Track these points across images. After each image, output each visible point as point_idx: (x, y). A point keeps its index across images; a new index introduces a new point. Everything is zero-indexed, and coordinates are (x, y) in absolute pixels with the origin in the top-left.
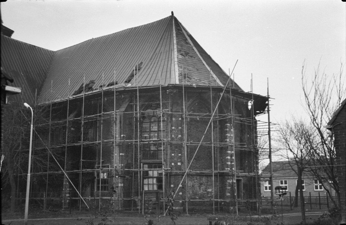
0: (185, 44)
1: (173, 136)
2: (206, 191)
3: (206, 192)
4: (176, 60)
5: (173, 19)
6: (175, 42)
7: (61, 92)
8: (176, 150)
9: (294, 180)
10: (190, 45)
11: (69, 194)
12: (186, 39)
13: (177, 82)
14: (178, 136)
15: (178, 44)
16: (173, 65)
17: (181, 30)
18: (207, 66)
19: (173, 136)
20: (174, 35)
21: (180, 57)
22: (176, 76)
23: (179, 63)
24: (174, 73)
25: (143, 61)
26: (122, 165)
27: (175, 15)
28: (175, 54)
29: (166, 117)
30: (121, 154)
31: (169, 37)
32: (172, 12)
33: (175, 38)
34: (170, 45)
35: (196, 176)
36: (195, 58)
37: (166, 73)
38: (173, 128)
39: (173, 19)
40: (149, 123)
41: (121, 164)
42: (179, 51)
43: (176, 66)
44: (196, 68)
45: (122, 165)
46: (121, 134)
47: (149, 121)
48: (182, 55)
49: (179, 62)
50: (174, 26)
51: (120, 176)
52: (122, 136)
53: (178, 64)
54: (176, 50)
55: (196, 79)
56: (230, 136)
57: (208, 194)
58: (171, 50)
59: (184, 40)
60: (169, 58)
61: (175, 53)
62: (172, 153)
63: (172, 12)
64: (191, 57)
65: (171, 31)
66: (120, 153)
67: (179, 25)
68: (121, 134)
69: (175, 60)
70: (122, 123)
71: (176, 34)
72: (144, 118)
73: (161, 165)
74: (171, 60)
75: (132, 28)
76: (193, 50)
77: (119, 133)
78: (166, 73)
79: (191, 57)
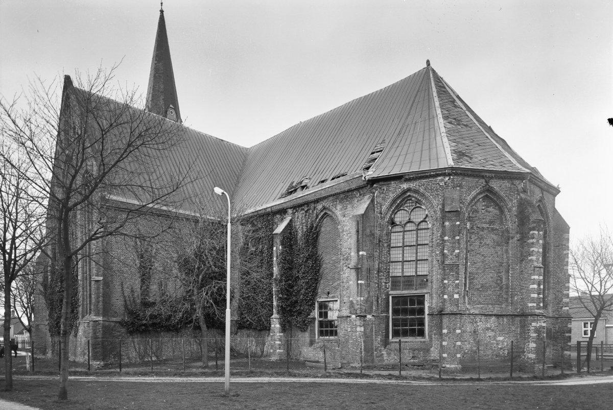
0: (454, 108)
1: (445, 251)
2: (495, 339)
3: (495, 342)
4: (443, 130)
5: (431, 72)
6: (437, 104)
7: (263, 196)
8: (451, 273)
9: (580, 322)
10: (462, 108)
11: (280, 340)
12: (454, 101)
13: (451, 163)
14: (454, 251)
15: (442, 106)
16: (438, 138)
17: (445, 88)
18: (492, 140)
19: (445, 251)
20: (435, 94)
21: (449, 126)
22: (447, 155)
23: (449, 135)
24: (443, 151)
25: (385, 139)
26: (362, 299)
27: (432, 65)
28: (440, 121)
29: (430, 223)
30: (359, 282)
31: (426, 97)
32: (428, 62)
33: (436, 99)
34: (429, 109)
35: (480, 316)
36: (471, 127)
37: (430, 151)
38: (446, 238)
39: (431, 72)
40: (402, 234)
41: (361, 297)
42: (446, 118)
43: (445, 140)
44: (477, 142)
45: (362, 299)
46: (358, 251)
47: (402, 230)
48: (450, 123)
49: (449, 133)
50: (432, 81)
51: (358, 316)
52: (361, 253)
53: (447, 136)
54: (440, 116)
55: (480, 158)
56: (538, 252)
57: (497, 344)
58: (431, 118)
59: (451, 101)
60: (431, 128)
61: (441, 122)
62: (445, 279)
63: (428, 62)
64: (466, 126)
65: (429, 89)
66: (358, 280)
67: (439, 80)
68: (358, 251)
69: (442, 131)
70: (360, 232)
71: (438, 92)
72: (395, 226)
73: (422, 299)
74: (435, 131)
75: (360, 98)
76: (467, 115)
77: (326, 266)
78: (430, 151)
79: (466, 126)
